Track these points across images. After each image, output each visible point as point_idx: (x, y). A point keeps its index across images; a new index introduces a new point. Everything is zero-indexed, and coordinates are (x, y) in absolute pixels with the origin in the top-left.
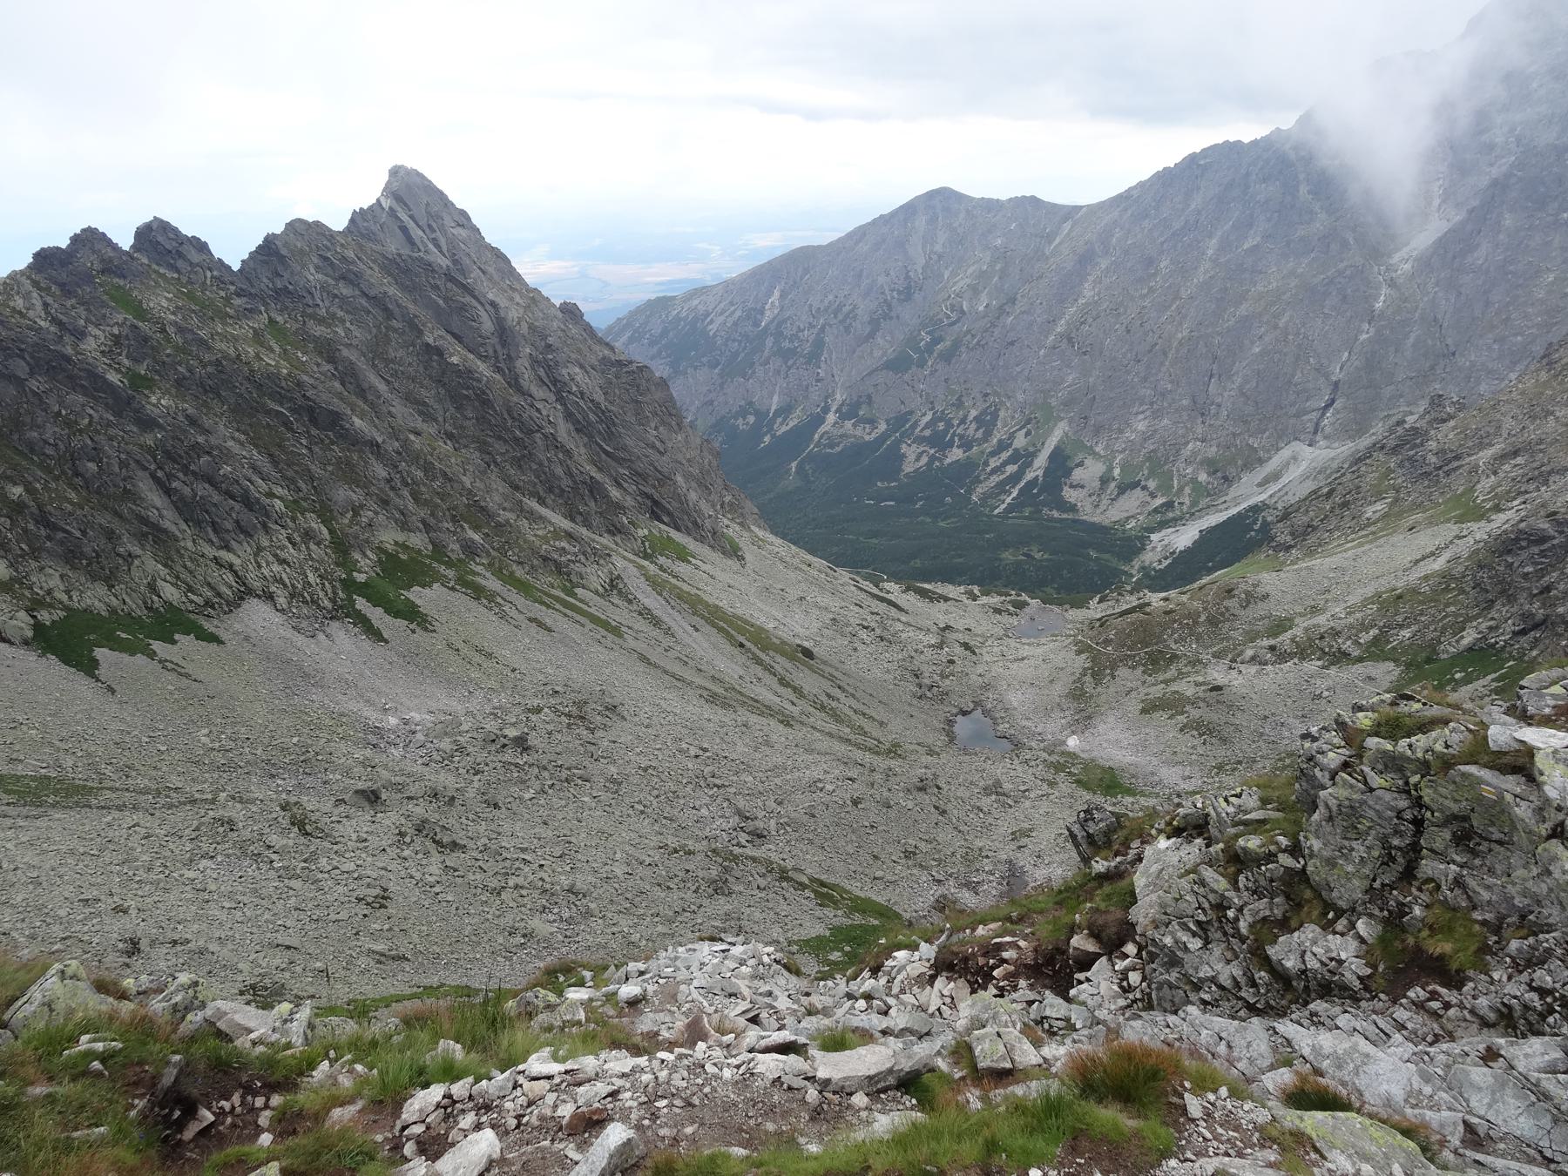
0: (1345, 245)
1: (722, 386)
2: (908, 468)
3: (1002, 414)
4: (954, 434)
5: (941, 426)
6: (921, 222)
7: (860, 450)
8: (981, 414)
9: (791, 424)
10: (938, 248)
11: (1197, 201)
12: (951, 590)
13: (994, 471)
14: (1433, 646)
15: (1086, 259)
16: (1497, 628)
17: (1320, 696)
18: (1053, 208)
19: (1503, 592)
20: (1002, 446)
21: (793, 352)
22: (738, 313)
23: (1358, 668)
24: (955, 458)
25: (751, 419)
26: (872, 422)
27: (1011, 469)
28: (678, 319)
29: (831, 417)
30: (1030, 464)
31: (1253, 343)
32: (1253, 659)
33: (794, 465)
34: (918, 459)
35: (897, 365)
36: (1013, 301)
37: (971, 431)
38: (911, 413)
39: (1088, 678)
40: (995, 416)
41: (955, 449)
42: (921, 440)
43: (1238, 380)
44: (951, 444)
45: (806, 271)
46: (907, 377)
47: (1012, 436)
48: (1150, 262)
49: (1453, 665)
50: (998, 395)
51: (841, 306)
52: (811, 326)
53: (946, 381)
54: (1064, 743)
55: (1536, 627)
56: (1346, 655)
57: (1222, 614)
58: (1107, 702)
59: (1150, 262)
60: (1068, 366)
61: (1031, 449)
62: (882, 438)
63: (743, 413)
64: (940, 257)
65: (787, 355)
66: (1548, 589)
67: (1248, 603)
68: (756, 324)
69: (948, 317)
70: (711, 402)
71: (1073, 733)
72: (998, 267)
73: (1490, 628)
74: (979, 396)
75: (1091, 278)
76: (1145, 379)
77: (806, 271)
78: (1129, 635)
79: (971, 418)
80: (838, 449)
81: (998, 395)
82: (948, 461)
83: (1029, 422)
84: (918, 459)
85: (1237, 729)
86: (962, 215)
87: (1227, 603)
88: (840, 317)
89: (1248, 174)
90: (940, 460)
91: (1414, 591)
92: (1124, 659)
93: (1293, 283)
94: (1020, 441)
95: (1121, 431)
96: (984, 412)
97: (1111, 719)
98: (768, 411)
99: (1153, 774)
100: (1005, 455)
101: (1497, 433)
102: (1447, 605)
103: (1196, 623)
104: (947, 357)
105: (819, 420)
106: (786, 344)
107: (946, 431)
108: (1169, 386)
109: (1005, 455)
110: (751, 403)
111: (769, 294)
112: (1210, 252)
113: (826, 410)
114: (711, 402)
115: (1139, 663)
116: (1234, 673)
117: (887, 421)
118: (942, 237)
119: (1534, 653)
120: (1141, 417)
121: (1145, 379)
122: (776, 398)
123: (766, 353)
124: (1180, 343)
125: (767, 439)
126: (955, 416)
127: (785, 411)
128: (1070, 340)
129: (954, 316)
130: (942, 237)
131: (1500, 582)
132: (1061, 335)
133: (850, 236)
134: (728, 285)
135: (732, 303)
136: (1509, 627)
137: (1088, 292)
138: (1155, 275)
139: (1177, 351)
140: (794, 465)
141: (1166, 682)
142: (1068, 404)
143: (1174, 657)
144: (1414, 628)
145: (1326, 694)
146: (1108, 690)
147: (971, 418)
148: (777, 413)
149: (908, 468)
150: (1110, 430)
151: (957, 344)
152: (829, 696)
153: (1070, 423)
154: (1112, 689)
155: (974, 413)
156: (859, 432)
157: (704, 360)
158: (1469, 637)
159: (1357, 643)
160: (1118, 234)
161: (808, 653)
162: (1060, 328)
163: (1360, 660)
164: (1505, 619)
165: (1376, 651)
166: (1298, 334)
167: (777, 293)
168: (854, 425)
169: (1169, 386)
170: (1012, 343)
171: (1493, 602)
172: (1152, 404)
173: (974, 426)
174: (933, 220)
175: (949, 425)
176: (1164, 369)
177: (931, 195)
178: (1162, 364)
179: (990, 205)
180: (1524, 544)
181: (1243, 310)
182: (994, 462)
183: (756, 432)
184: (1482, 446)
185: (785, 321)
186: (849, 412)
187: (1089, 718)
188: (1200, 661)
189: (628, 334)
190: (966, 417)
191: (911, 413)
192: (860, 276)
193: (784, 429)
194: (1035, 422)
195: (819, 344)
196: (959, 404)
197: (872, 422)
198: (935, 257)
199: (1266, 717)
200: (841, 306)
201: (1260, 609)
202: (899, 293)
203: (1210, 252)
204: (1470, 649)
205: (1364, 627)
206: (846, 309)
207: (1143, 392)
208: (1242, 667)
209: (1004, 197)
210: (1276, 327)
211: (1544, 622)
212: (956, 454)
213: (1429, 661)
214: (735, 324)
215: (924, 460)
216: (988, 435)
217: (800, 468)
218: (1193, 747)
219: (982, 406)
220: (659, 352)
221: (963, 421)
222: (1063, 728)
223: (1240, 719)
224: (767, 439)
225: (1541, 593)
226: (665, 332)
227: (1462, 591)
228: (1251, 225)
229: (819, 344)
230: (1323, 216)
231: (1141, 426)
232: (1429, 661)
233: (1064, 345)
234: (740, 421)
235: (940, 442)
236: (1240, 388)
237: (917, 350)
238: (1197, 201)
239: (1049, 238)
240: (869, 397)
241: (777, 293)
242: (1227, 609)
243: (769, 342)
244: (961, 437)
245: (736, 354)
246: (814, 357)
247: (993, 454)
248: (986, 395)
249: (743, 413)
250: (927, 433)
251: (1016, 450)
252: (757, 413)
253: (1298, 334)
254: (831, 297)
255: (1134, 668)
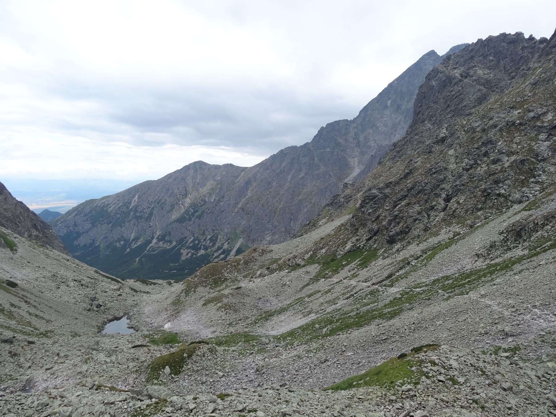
0: (330, 176)
1: (111, 231)
2: (183, 258)
3: (219, 237)
4: (201, 245)
5: (197, 242)
6: (191, 172)
7: (165, 252)
8: (212, 237)
9: (138, 244)
10: (198, 180)
11: (284, 164)
12: (160, 281)
13: (216, 257)
14: (334, 254)
15: (248, 183)
16: (360, 239)
17: (285, 284)
18: (238, 168)
19: (361, 224)
20: (219, 248)
21: (141, 217)
22: (121, 204)
23: (304, 269)
24: (201, 254)
25: (122, 243)
26: (170, 242)
27: (222, 256)
28: (97, 206)
29: (155, 241)
30: (229, 254)
31: (304, 208)
32: (260, 275)
33: (137, 259)
34: (187, 255)
35: (180, 220)
36: (223, 197)
37: (208, 244)
38: (185, 238)
39: (183, 294)
40: (217, 238)
41: (202, 251)
42: (188, 248)
43: (300, 221)
44: (200, 248)
45: (149, 189)
46: (184, 225)
47: (223, 244)
48: (269, 183)
49: (342, 260)
50: (218, 230)
51: (160, 201)
52: (148, 207)
53: (199, 226)
54: (163, 326)
55: (375, 234)
56: (298, 265)
57: (251, 259)
58: (190, 304)
59: (269, 183)
60: (242, 219)
61: (230, 249)
62: (174, 247)
63: (119, 240)
64: (198, 184)
65: (137, 218)
66: (378, 217)
67: (263, 254)
68: (128, 208)
69: (200, 203)
70: (107, 237)
71: (169, 321)
72: (219, 187)
73: (357, 240)
74: (211, 231)
75: (250, 189)
76: (269, 222)
77: (149, 189)
78: (206, 272)
79: (208, 239)
80: (156, 252)
81: (218, 230)
82: (199, 254)
83: (229, 239)
84: (187, 255)
85: (244, 304)
86: (206, 170)
87: (253, 255)
88: (160, 204)
89: (299, 155)
90: (195, 254)
91: (329, 235)
92: (201, 283)
93: (316, 188)
94: (226, 246)
95: (261, 241)
96: (213, 237)
97: (189, 312)
98: (130, 239)
99: (197, 333)
100: (220, 252)
101: (364, 186)
102: (340, 236)
103: (238, 264)
104: (199, 217)
105: (150, 242)
106: (138, 214)
107: (198, 244)
108: (277, 224)
109: (220, 252)
110: (123, 237)
111: (134, 196)
112: (289, 180)
113: (153, 238)
114: (107, 237)
115: (208, 284)
116: (251, 283)
117: (176, 241)
118: (199, 177)
119: (375, 246)
120: (268, 235)
121: (269, 222)
122: (133, 235)
123: (130, 218)
124: (280, 209)
125: (128, 250)
126: (202, 238)
127: (136, 239)
128: (243, 209)
129: (202, 203)
130: (199, 177)
131: (360, 220)
132: (240, 208)
133: (165, 177)
134: (118, 195)
135: (119, 200)
136: (365, 237)
137: (249, 194)
138: (271, 187)
139: (279, 212)
140: (137, 259)
141: (219, 291)
142: (242, 232)
143: (226, 279)
144: (327, 248)
145: (288, 283)
146: (193, 297)
147: (208, 239)
148: (133, 240)
149: (183, 258)
150: (258, 240)
151: (203, 213)
152: (12, 305)
153: (244, 238)
154: (193, 298)
155: (209, 237)
156: (165, 246)
157: (105, 221)
158: (349, 246)
159: (304, 259)
160: (259, 175)
161: (13, 285)
162: (240, 205)
163: (304, 266)
164: (363, 234)
165: (311, 261)
166: (318, 205)
167: (137, 197)
168: (163, 243)
169: (277, 224)
170: (223, 211)
171: (357, 229)
172: (272, 230)
173: (209, 242)
174: (196, 171)
175: (200, 242)
176: (275, 218)
177: (195, 163)
178: (274, 216)
179: (216, 167)
180: (367, 201)
181: (300, 197)
182: (216, 254)
183: (124, 248)
184: (359, 192)
185: (139, 206)
186: (162, 238)
187: (179, 312)
188: (237, 280)
189: (75, 213)
190: (206, 238)
191: (185, 238)
192: (168, 189)
193: (136, 246)
194: (231, 239)
195: (151, 214)
196: (204, 234)
197: (170, 242)
198: (196, 184)
199: (260, 298)
200: (160, 201)
201: (268, 256)
202: (183, 195)
203: (289, 180)
204: (349, 251)
205: (307, 252)
206: (162, 201)
207: (268, 226)
208: (255, 280)
209: (221, 164)
210: (311, 203)
211: (378, 231)
212: (202, 252)
213: (333, 260)
214: (119, 208)
215: (190, 255)
216: (214, 245)
217: (140, 260)
218: (221, 317)
219: (212, 234)
220: (88, 218)
221: (205, 240)
222: (165, 319)
223: (247, 300)
224: (128, 250)
225: (376, 220)
226: (91, 212)
227: (347, 229)
228: (301, 171)
229: (151, 214)
230: (323, 167)
231: (268, 239)
232: (333, 260)
233: (241, 211)
234: (118, 244)
235: (196, 248)
236: (301, 224)
237: (188, 215)
238: (284, 164)
239: (237, 177)
240: (170, 233)
241: (137, 197)
242: (253, 257)
243: (132, 213)
244: (204, 246)
245: (119, 218)
246: (148, 219)
247: (216, 251)
248: (214, 230)
249: (119, 240)
250: (191, 245)
251: (224, 249)
252: (125, 241)
253: (318, 205)
254: (157, 197)
255: (206, 286)
